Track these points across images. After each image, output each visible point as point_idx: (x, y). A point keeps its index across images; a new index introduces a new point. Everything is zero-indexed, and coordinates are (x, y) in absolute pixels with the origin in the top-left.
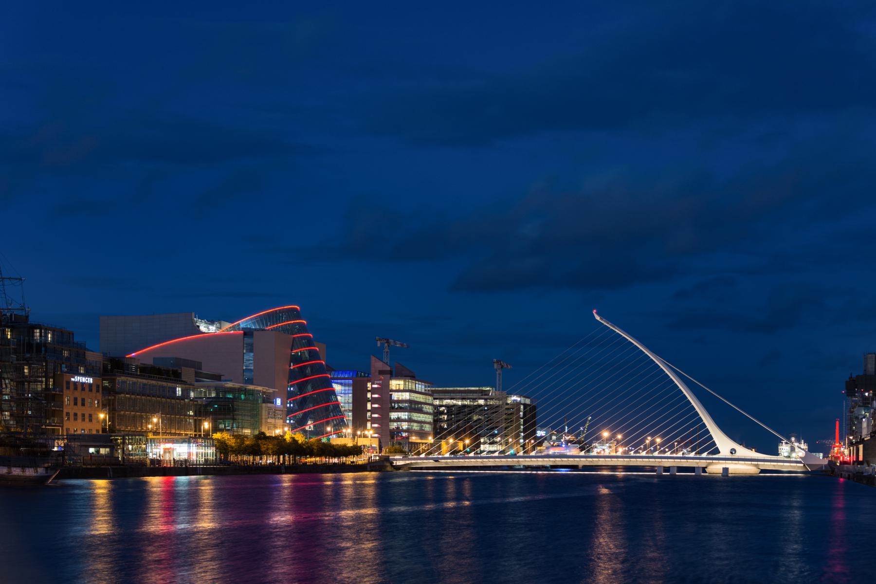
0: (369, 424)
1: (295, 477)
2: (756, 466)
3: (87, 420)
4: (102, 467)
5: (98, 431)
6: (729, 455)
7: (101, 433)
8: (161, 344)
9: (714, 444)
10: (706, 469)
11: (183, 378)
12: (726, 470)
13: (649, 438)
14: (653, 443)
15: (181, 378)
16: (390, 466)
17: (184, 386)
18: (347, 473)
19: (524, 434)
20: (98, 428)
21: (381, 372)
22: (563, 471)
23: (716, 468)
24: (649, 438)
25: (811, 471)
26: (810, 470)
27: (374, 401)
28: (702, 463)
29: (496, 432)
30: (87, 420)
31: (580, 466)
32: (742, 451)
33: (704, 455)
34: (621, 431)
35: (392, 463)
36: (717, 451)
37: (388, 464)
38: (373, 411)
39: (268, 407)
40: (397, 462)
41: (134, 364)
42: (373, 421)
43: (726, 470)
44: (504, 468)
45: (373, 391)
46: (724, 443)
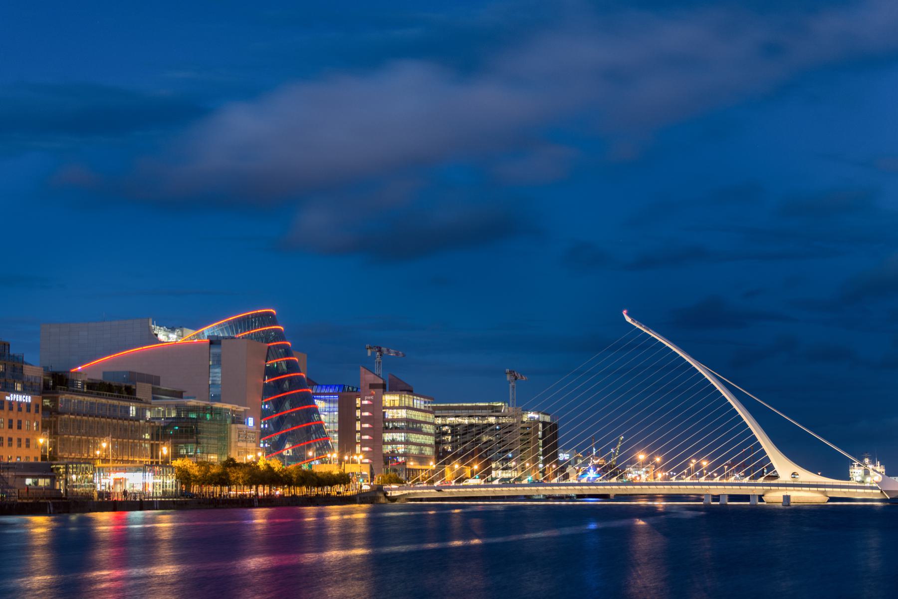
0: (358, 448)
3: (24, 445)
5: (36, 459)
7: (39, 461)
9: (771, 468)
11: (138, 396)
12: (787, 498)
13: (694, 461)
14: (698, 467)
15: (136, 395)
16: (384, 498)
20: (36, 456)
21: (373, 386)
22: (592, 502)
23: (775, 497)
24: (58, 483)
26: (889, 498)
27: (364, 420)
30: (24, 445)
32: (806, 476)
33: (761, 480)
34: (659, 453)
35: (385, 494)
37: (381, 495)
38: (363, 431)
39: (238, 429)
40: (393, 492)
42: (364, 443)
43: (787, 498)
45: (363, 408)
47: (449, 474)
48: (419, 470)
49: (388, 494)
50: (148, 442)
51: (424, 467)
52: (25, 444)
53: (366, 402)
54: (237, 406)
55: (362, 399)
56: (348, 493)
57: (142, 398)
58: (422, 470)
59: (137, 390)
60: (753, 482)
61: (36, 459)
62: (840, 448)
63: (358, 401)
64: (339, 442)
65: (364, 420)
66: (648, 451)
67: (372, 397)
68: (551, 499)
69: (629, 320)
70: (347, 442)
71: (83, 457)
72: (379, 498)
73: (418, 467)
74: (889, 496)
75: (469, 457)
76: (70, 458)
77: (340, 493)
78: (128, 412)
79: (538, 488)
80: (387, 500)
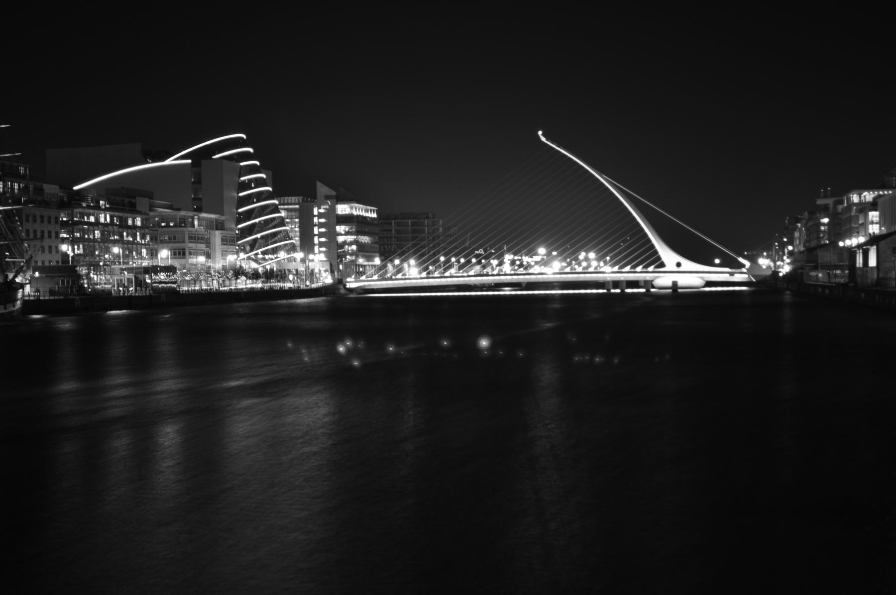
0: (316, 249)
1: (328, 301)
2: (702, 278)
3: (47, 251)
4: (70, 297)
5: (57, 262)
6: (676, 269)
7: (60, 264)
8: (5, 208)
9: (659, 258)
10: (12, 304)
11: (138, 208)
12: (675, 284)
15: (136, 208)
16: (343, 289)
17: (144, 217)
18: (297, 299)
19: (445, 257)
20: (57, 260)
21: (327, 197)
22: (507, 292)
23: (664, 281)
25: (756, 281)
26: (754, 280)
27: (320, 225)
28: (648, 276)
29: (493, 251)
30: (47, 251)
31: (524, 285)
32: (687, 265)
33: (651, 269)
34: (555, 250)
35: (345, 285)
36: (662, 265)
37: (341, 287)
38: (321, 235)
40: (351, 284)
41: (90, 196)
42: (321, 244)
43: (675, 284)
44: (447, 289)
45: (320, 216)
46: (669, 256)
47: (390, 267)
48: (366, 265)
49: (346, 285)
50: (144, 246)
51: (370, 263)
52: (48, 249)
53: (322, 211)
54: (219, 216)
55: (319, 208)
56: (314, 286)
57: (141, 210)
58: (369, 266)
59: (137, 204)
60: (644, 270)
61: (57, 262)
62: (724, 246)
63: (316, 211)
64: (300, 244)
65: (320, 225)
66: (547, 247)
67: (327, 207)
68: (484, 289)
69: (543, 139)
70: (307, 244)
71: (96, 260)
72: (339, 289)
73: (366, 263)
74: (755, 279)
75: (65, 241)
76: (86, 261)
77: (308, 286)
78: (127, 221)
79: (267, 286)
80: (346, 290)
